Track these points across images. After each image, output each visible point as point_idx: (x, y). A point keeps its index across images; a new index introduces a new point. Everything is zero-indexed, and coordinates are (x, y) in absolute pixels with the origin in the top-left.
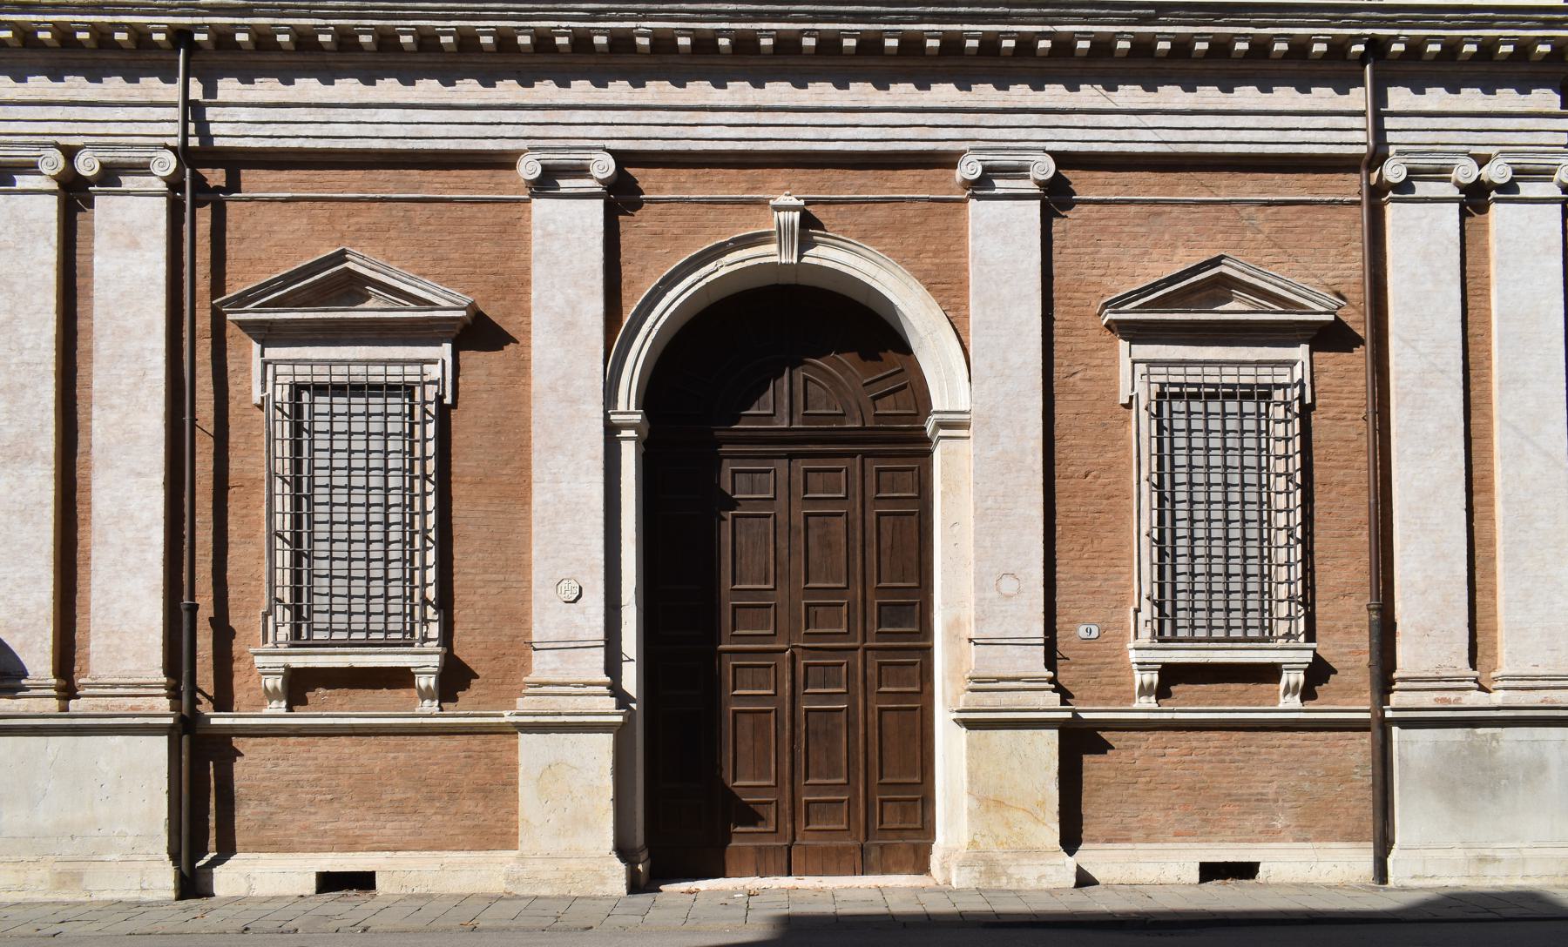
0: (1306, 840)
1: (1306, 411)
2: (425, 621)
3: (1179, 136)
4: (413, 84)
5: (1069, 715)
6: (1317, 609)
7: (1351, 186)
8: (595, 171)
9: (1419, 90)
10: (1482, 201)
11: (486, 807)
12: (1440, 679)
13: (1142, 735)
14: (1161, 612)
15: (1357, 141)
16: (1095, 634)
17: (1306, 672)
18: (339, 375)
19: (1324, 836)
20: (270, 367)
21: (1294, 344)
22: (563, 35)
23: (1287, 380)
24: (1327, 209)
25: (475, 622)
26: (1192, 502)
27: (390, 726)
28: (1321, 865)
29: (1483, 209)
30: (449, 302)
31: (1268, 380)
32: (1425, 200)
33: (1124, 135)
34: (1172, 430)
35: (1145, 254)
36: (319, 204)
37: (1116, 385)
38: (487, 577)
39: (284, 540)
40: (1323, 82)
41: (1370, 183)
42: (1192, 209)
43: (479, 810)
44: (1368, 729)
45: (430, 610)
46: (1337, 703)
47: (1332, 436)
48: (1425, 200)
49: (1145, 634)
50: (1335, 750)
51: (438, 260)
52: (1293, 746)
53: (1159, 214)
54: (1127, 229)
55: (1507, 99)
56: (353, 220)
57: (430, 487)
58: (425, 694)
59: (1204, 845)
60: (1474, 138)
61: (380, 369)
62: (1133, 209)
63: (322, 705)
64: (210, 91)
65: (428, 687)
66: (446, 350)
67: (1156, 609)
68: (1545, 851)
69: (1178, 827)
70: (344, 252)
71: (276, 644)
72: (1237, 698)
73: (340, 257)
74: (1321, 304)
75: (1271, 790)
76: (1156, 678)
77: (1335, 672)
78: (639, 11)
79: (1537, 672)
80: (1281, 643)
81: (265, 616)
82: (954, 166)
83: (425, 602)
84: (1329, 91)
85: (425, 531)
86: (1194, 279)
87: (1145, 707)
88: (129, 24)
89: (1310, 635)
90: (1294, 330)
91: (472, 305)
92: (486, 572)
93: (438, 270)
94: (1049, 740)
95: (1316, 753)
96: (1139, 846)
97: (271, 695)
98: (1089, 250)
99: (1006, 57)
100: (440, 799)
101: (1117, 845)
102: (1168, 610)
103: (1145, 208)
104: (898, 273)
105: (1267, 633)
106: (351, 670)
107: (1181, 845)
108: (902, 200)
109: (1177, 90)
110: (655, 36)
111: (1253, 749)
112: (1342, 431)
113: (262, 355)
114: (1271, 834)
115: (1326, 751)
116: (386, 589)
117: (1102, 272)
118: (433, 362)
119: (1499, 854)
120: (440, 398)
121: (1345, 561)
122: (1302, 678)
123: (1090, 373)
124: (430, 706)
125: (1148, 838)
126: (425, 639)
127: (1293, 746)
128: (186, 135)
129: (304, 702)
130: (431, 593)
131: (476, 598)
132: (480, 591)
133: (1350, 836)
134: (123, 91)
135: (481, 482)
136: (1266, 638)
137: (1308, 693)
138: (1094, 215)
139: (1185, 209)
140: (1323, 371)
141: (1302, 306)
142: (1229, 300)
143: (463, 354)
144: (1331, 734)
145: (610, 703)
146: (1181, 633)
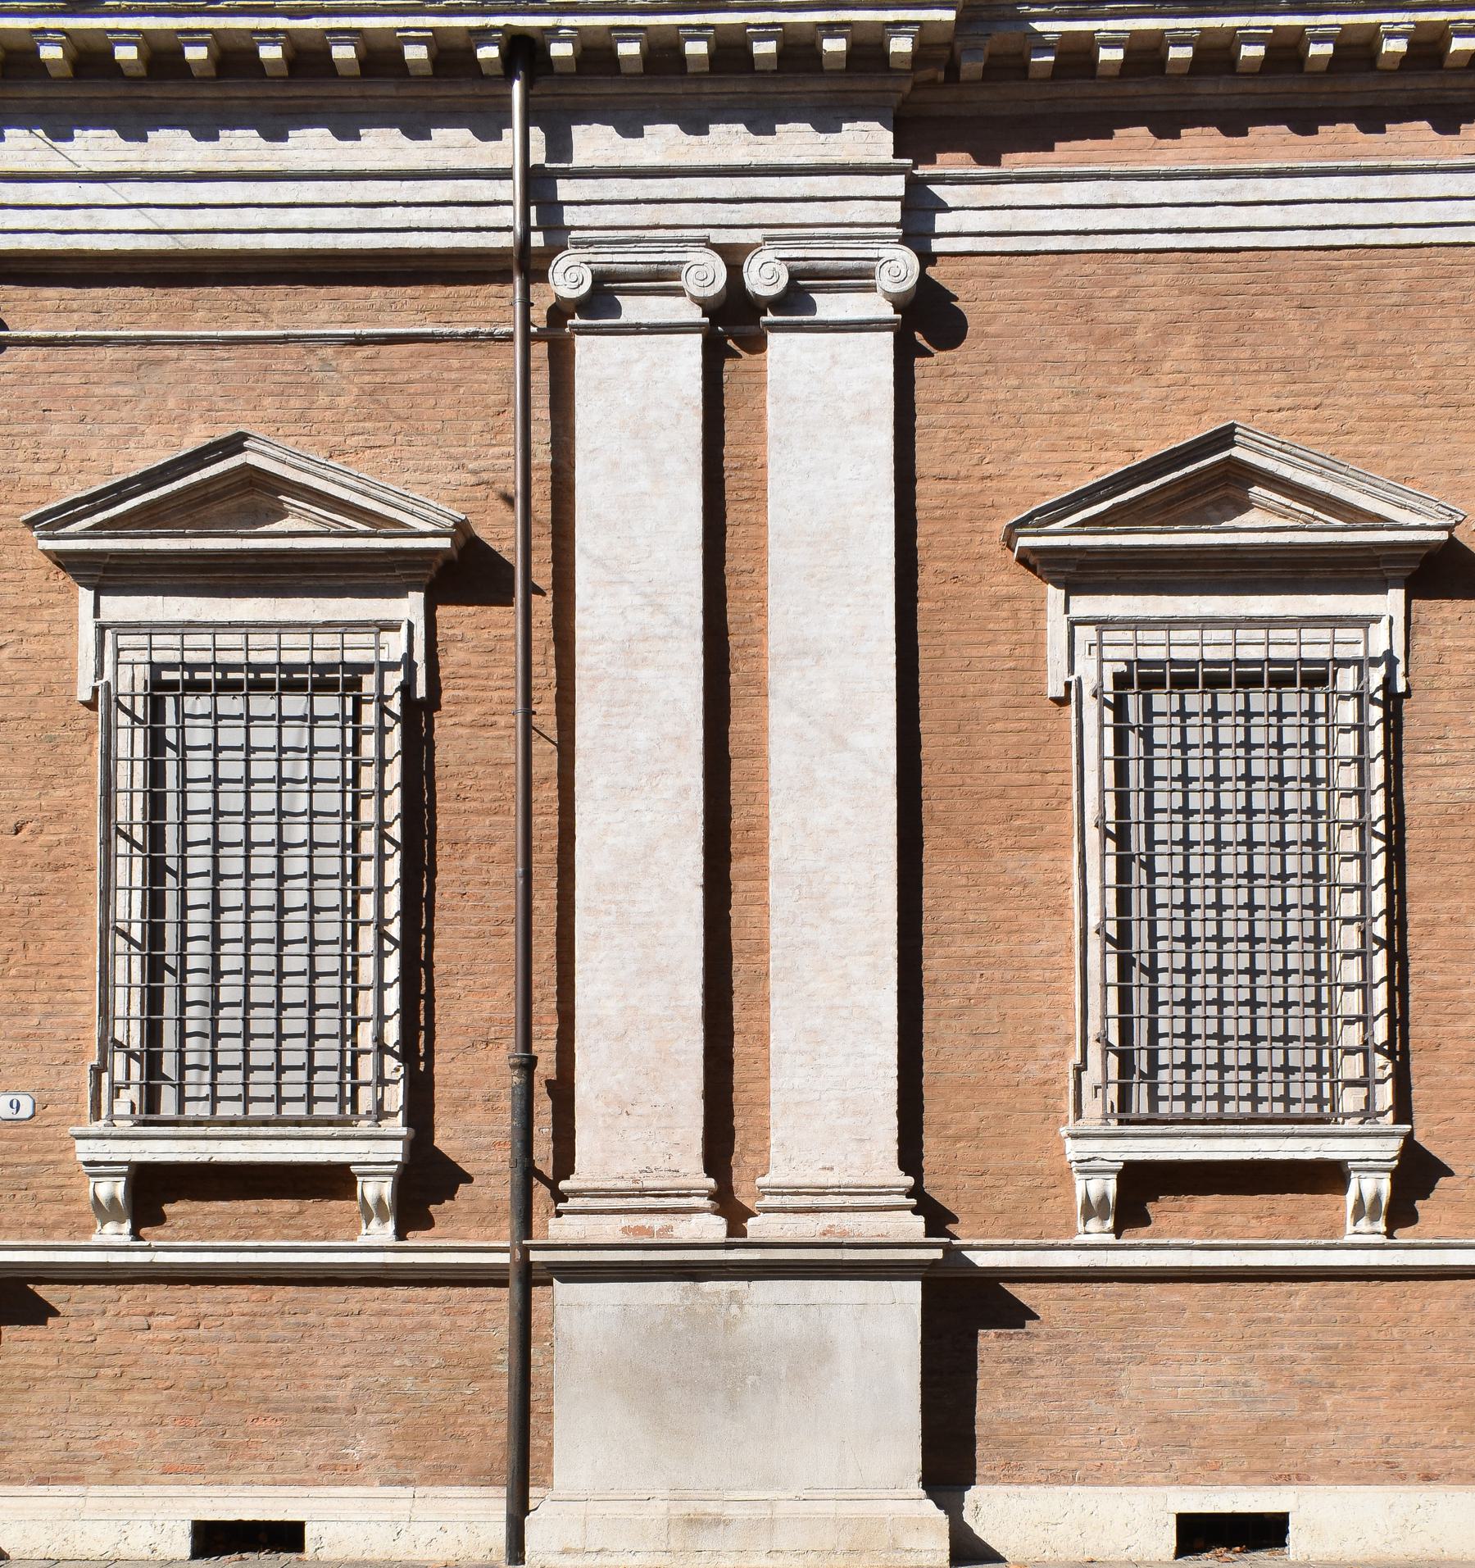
0: (404, 1482)
1: (1393, 702)
2: (382, 1081)
3: (178, 219)
4: (285, 138)
5: (938, 1254)
6: (437, 1069)
7: (494, 307)
8: (692, 283)
9: (631, 129)
10: (750, 329)
12: (642, 1193)
13: (110, 1291)
15: (497, 221)
16: (26, 1111)
17: (1396, 1175)
18: (1217, 647)
19: (440, 1475)
20: (108, 633)
21: (397, 591)
22: (1110, 44)
23: (1358, 651)
24: (469, 352)
26: (217, 877)
27: (385, 1266)
28: (416, 1529)
29: (757, 345)
31: (1322, 653)
32: (637, 329)
33: (77, 219)
34: (183, 748)
35: (131, 434)
37: (73, 669)
40: (451, 118)
41: (534, 300)
42: (220, 352)
44: (503, 1283)
45: (391, 1063)
46: (471, 1233)
47: (470, 757)
48: (637, 329)
49: (1093, 1107)
50: (461, 1321)
52: (385, 1313)
53: (159, 363)
54: (98, 391)
55: (795, 141)
57: (1377, 844)
59: (214, 1490)
60: (723, 214)
62: (109, 353)
64: (559, 147)
65: (113, 1199)
66: (1397, 596)
68: (820, 1507)
69: (171, 1458)
71: (112, 1118)
72: (282, 1226)
73: (1224, 437)
74: (426, 520)
75: (341, 1394)
76: (1112, 1188)
77: (468, 1179)
79: (831, 1179)
81: (97, 1072)
83: (382, 1049)
84: (464, 135)
85: (381, 922)
86: (195, 477)
87: (1093, 1243)
88: (284, 31)
89: (1403, 1110)
90: (391, 567)
91: (462, 527)
94: (906, 1299)
95: (427, 1326)
96: (95, 1490)
97: (104, 1211)
98: (29, 428)
99: (1315, 74)
101: (54, 1490)
103: (132, 353)
105: (1327, 1109)
107: (173, 1490)
109: (183, 137)
110: (437, 41)
111: (312, 1318)
112: (474, 746)
113: (97, 614)
114: (338, 1471)
115: (446, 1322)
116: (311, 1022)
117: (52, 466)
118: (391, 626)
119: (732, 1511)
120: (407, 688)
121: (489, 979)
122: (1385, 1186)
123: (28, 648)
125: (115, 1477)
126: (380, 1113)
127: (385, 1313)
128: (527, 230)
129: (159, 1219)
130: (392, 1033)
133: (482, 1478)
134: (266, 154)
136: (1324, 1117)
137: (1400, 1213)
138: (40, 366)
139: (205, 353)
140: (453, 640)
142: (282, 514)
143: (442, 611)
144: (456, 1292)
145: (914, 1226)
146: (192, 1110)
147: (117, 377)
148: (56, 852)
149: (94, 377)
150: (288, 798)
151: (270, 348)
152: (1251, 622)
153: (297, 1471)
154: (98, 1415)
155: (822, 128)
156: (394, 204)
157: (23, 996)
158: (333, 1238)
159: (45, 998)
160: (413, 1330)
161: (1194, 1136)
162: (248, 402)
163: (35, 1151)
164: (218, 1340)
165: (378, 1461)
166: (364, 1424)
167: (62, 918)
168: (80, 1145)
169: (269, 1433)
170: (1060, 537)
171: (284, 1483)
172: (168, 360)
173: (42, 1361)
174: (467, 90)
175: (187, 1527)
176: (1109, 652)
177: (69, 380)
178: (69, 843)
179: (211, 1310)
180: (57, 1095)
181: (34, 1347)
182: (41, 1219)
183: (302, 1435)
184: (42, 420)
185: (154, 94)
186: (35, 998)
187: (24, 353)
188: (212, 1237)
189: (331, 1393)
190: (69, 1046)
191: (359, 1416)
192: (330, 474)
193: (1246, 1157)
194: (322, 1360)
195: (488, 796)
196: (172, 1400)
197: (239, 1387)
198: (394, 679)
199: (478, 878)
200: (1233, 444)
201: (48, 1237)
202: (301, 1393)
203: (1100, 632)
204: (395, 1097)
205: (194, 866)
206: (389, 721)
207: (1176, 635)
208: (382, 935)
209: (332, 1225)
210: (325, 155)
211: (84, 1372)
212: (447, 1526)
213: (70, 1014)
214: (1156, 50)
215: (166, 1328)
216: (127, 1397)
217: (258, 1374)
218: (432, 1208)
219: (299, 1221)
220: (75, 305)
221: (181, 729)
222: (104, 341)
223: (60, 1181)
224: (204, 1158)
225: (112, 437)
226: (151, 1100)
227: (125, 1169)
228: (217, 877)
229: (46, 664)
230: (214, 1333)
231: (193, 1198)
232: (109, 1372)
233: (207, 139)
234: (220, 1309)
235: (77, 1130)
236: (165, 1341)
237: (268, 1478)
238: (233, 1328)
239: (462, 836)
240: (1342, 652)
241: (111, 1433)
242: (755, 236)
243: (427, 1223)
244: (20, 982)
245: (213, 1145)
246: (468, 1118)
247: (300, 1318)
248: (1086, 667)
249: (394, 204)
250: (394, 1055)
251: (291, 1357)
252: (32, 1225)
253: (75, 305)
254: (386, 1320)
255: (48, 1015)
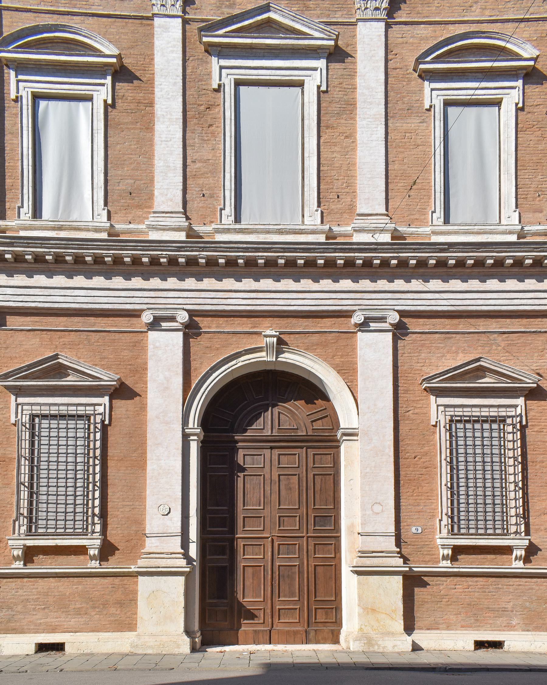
0: (528, 631)
5: (407, 569)
6: (531, 521)
8: (179, 319)
11: (121, 611)
14: (452, 521)
16: (420, 531)
20: (20, 407)
21: (517, 397)
22: (89, 256)
24: (533, 335)
25: (118, 524)
28: (536, 643)
30: (108, 377)
31: (504, 414)
33: (433, 302)
36: (45, 332)
38: (124, 503)
39: (25, 486)
42: (466, 335)
43: (118, 612)
45: (96, 519)
47: (537, 440)
49: (445, 531)
50: (541, 587)
51: (103, 359)
52: (520, 585)
54: (434, 345)
56: (62, 340)
57: (97, 462)
58: (92, 558)
59: (476, 632)
61: (65, 408)
62: (437, 336)
63: (41, 563)
65: (94, 555)
66: (106, 400)
67: (450, 520)
69: (463, 623)
70: (57, 355)
72: (491, 561)
73: (56, 357)
74: (530, 379)
75: (509, 606)
78: (200, 247)
80: (512, 536)
81: (14, 522)
82: (351, 317)
83: (94, 515)
86: (467, 368)
89: (527, 532)
91: (119, 379)
92: (124, 501)
93: (103, 363)
95: (532, 589)
96: (443, 632)
97: (16, 558)
98: (416, 355)
100: (98, 607)
102: (456, 520)
103: (443, 335)
104: (324, 365)
105: (505, 531)
106: (57, 547)
107: (464, 632)
108: (326, 332)
109: (459, 282)
111: (500, 586)
113: (16, 401)
114: (510, 627)
115: (537, 588)
117: (423, 364)
118: (101, 405)
120: (103, 421)
124: (95, 563)
125: (448, 628)
127: (520, 585)
131: (118, 513)
132: (121, 510)
134: (481, 286)
135: (122, 460)
136: (505, 534)
137: (527, 560)
141: (521, 380)
142: (484, 377)
145: (183, 562)
146: (463, 531)
147: (439, 341)
148: (426, 463)
149: (433, 342)
150: (66, 449)
151: (480, 335)
152: (55, 405)
153: (498, 627)
154: (442, 611)
155: (87, 278)
156: (518, 299)
157: (418, 501)
158: (505, 565)
159: (424, 501)
160: (528, 590)
161: (60, 539)
162: (474, 348)
163: (422, 541)
164: (474, 592)
165: (520, 625)
166: (516, 614)
167: (428, 481)
168: (10, 542)
169: (490, 617)
170: (434, 384)
171: (495, 630)
172: (452, 337)
173: (426, 597)
174: (537, 270)
175: (473, 642)
176: (447, 413)
177: (426, 342)
178: (429, 461)
179: (472, 584)
180: (428, 527)
181: (424, 593)
182: (425, 560)
183: (499, 617)
184: (419, 353)
185: (474, 271)
186: (421, 501)
187: (414, 336)
188: (472, 565)
189: (506, 606)
190: (431, 514)
191: (514, 612)
192: (504, 368)
193: (78, 544)
194: (503, 597)
195: (541, 450)
196: (463, 608)
197: (481, 604)
198: (99, 418)
199: (540, 471)
200: (59, 358)
201: (427, 564)
202: (498, 606)
203: (445, 408)
204: (98, 528)
205: (461, 467)
206: (97, 430)
207: (465, 409)
208: (94, 485)
209: (504, 562)
210: (497, 286)
211: (438, 600)
212: (545, 643)
213: (431, 505)
214: (353, 261)
215: (460, 588)
216: (450, 607)
217: (486, 601)
218: (531, 558)
219: (495, 560)
220: (428, 323)
221: (456, 433)
222: (436, 333)
223: (429, 549)
224: (474, 544)
225: (438, 357)
226: (30, 529)
227: (452, 547)
228: (467, 470)
229: (422, 415)
230: (473, 590)
231: (465, 554)
232: (445, 600)
233: (219, 281)
234: (475, 584)
235: (9, 538)
236: (460, 592)
237: (490, 629)
238: (478, 588)
239: (535, 460)
240: (509, 414)
241: (446, 617)
242: (144, 307)
243: (32, 562)
244: (417, 497)
245: (477, 541)
246: (540, 534)
247: (497, 586)
248: (441, 418)
249: (518, 299)
250: (97, 516)
251: (495, 597)
252: (422, 561)
253: (428, 323)
254: (520, 587)
255: (425, 506)
